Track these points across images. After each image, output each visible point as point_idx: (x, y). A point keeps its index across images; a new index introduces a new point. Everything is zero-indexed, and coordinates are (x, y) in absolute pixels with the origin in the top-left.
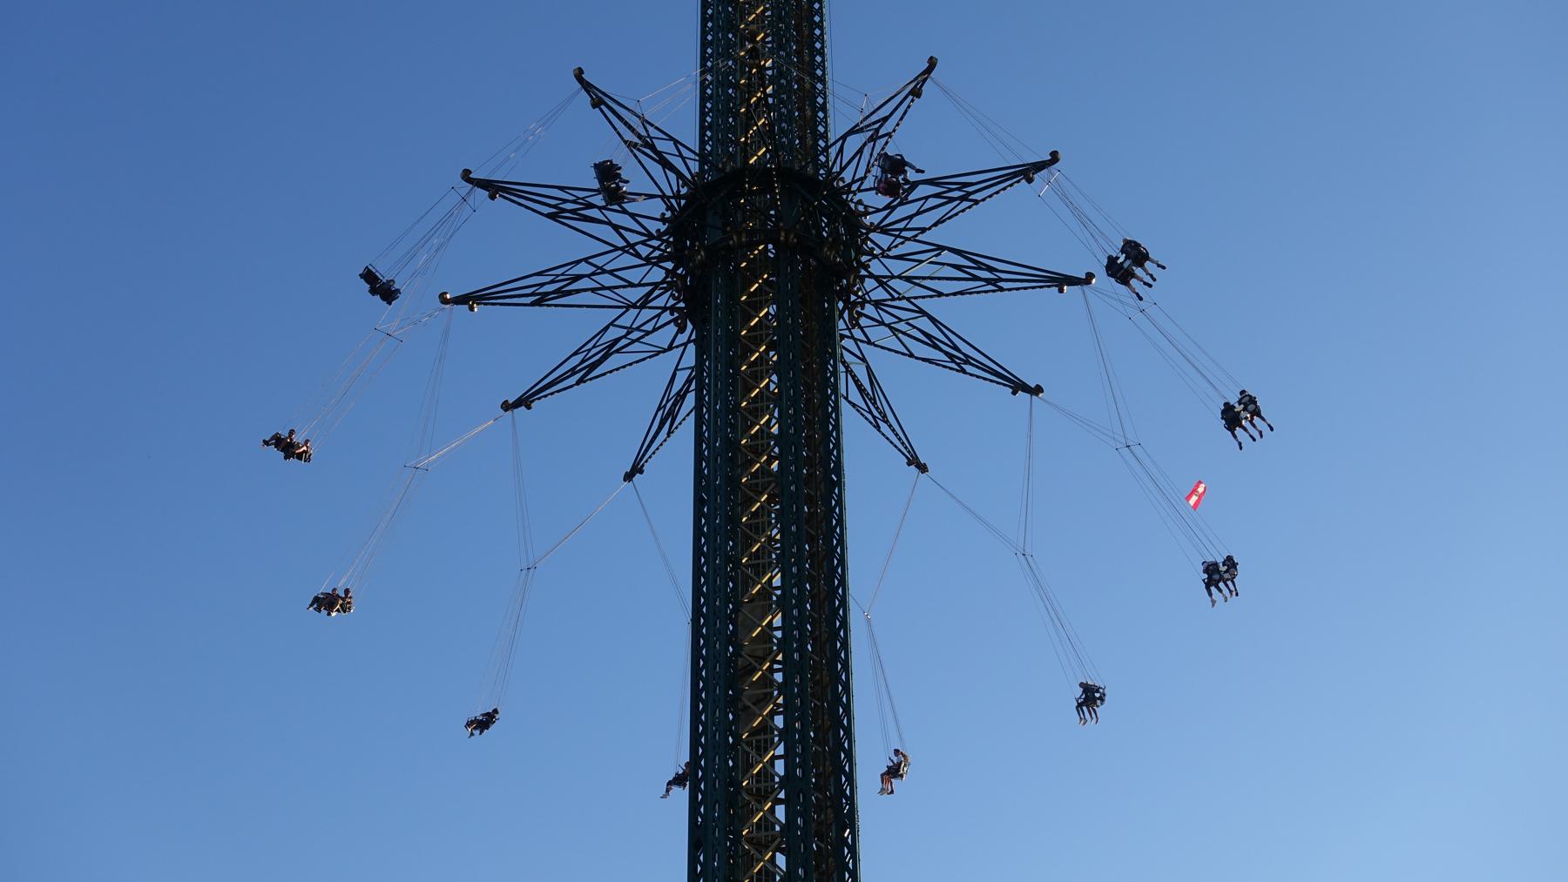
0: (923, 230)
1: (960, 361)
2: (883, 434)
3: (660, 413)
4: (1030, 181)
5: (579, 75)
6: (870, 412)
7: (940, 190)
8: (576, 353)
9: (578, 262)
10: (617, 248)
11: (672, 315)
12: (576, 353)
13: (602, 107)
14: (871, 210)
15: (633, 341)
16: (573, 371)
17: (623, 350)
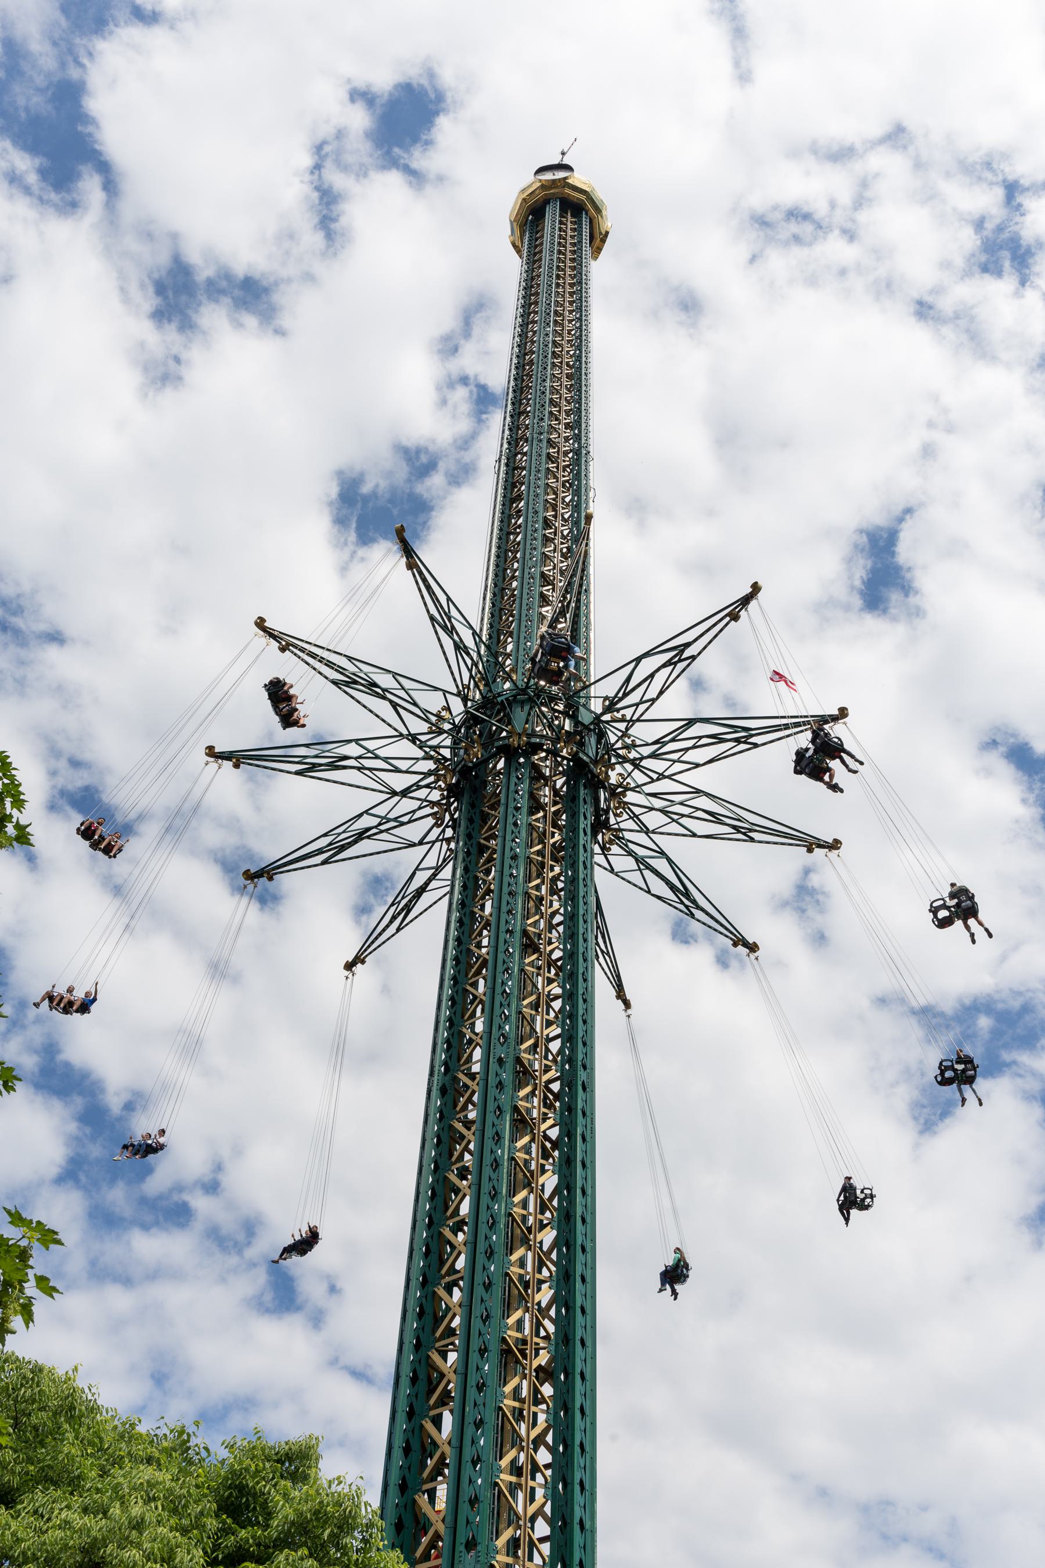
1: (745, 832)
2: (699, 921)
3: (393, 909)
5: (260, 623)
6: (682, 903)
8: (325, 835)
9: (360, 815)
10: (401, 735)
11: (433, 808)
12: (325, 835)
13: (291, 647)
14: (638, 742)
15: (382, 832)
16: (320, 851)
17: (374, 837)
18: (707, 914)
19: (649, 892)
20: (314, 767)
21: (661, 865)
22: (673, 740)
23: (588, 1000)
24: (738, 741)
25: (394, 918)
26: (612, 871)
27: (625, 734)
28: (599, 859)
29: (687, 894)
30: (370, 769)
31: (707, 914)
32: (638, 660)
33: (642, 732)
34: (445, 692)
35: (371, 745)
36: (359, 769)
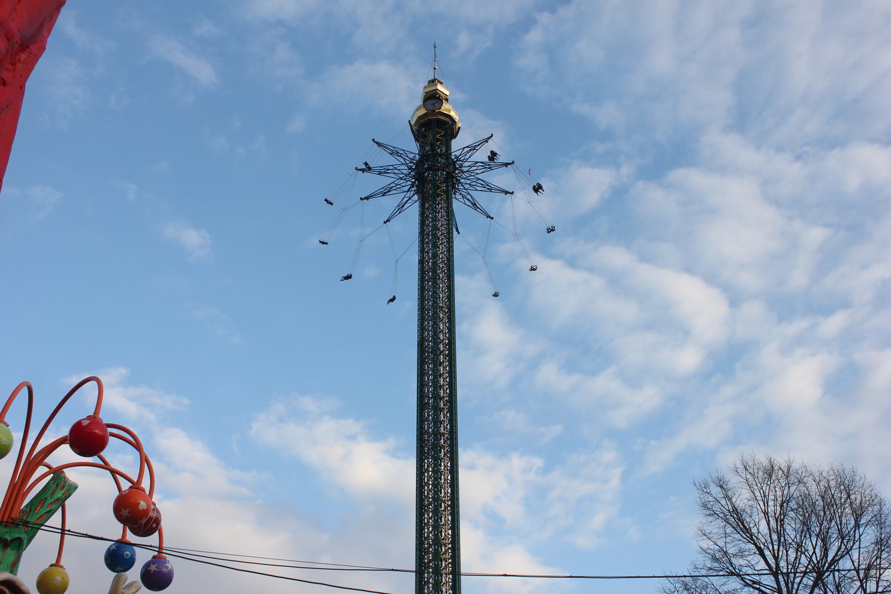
0: (467, 159)
1: (490, 190)
4: (507, 167)
5: (373, 140)
7: (483, 165)
9: (391, 184)
18: (480, 209)
20: (385, 193)
21: (469, 197)
22: (474, 166)
24: (489, 189)
25: (398, 210)
26: (456, 199)
28: (453, 196)
29: (475, 205)
31: (480, 209)
32: (464, 148)
35: (395, 166)
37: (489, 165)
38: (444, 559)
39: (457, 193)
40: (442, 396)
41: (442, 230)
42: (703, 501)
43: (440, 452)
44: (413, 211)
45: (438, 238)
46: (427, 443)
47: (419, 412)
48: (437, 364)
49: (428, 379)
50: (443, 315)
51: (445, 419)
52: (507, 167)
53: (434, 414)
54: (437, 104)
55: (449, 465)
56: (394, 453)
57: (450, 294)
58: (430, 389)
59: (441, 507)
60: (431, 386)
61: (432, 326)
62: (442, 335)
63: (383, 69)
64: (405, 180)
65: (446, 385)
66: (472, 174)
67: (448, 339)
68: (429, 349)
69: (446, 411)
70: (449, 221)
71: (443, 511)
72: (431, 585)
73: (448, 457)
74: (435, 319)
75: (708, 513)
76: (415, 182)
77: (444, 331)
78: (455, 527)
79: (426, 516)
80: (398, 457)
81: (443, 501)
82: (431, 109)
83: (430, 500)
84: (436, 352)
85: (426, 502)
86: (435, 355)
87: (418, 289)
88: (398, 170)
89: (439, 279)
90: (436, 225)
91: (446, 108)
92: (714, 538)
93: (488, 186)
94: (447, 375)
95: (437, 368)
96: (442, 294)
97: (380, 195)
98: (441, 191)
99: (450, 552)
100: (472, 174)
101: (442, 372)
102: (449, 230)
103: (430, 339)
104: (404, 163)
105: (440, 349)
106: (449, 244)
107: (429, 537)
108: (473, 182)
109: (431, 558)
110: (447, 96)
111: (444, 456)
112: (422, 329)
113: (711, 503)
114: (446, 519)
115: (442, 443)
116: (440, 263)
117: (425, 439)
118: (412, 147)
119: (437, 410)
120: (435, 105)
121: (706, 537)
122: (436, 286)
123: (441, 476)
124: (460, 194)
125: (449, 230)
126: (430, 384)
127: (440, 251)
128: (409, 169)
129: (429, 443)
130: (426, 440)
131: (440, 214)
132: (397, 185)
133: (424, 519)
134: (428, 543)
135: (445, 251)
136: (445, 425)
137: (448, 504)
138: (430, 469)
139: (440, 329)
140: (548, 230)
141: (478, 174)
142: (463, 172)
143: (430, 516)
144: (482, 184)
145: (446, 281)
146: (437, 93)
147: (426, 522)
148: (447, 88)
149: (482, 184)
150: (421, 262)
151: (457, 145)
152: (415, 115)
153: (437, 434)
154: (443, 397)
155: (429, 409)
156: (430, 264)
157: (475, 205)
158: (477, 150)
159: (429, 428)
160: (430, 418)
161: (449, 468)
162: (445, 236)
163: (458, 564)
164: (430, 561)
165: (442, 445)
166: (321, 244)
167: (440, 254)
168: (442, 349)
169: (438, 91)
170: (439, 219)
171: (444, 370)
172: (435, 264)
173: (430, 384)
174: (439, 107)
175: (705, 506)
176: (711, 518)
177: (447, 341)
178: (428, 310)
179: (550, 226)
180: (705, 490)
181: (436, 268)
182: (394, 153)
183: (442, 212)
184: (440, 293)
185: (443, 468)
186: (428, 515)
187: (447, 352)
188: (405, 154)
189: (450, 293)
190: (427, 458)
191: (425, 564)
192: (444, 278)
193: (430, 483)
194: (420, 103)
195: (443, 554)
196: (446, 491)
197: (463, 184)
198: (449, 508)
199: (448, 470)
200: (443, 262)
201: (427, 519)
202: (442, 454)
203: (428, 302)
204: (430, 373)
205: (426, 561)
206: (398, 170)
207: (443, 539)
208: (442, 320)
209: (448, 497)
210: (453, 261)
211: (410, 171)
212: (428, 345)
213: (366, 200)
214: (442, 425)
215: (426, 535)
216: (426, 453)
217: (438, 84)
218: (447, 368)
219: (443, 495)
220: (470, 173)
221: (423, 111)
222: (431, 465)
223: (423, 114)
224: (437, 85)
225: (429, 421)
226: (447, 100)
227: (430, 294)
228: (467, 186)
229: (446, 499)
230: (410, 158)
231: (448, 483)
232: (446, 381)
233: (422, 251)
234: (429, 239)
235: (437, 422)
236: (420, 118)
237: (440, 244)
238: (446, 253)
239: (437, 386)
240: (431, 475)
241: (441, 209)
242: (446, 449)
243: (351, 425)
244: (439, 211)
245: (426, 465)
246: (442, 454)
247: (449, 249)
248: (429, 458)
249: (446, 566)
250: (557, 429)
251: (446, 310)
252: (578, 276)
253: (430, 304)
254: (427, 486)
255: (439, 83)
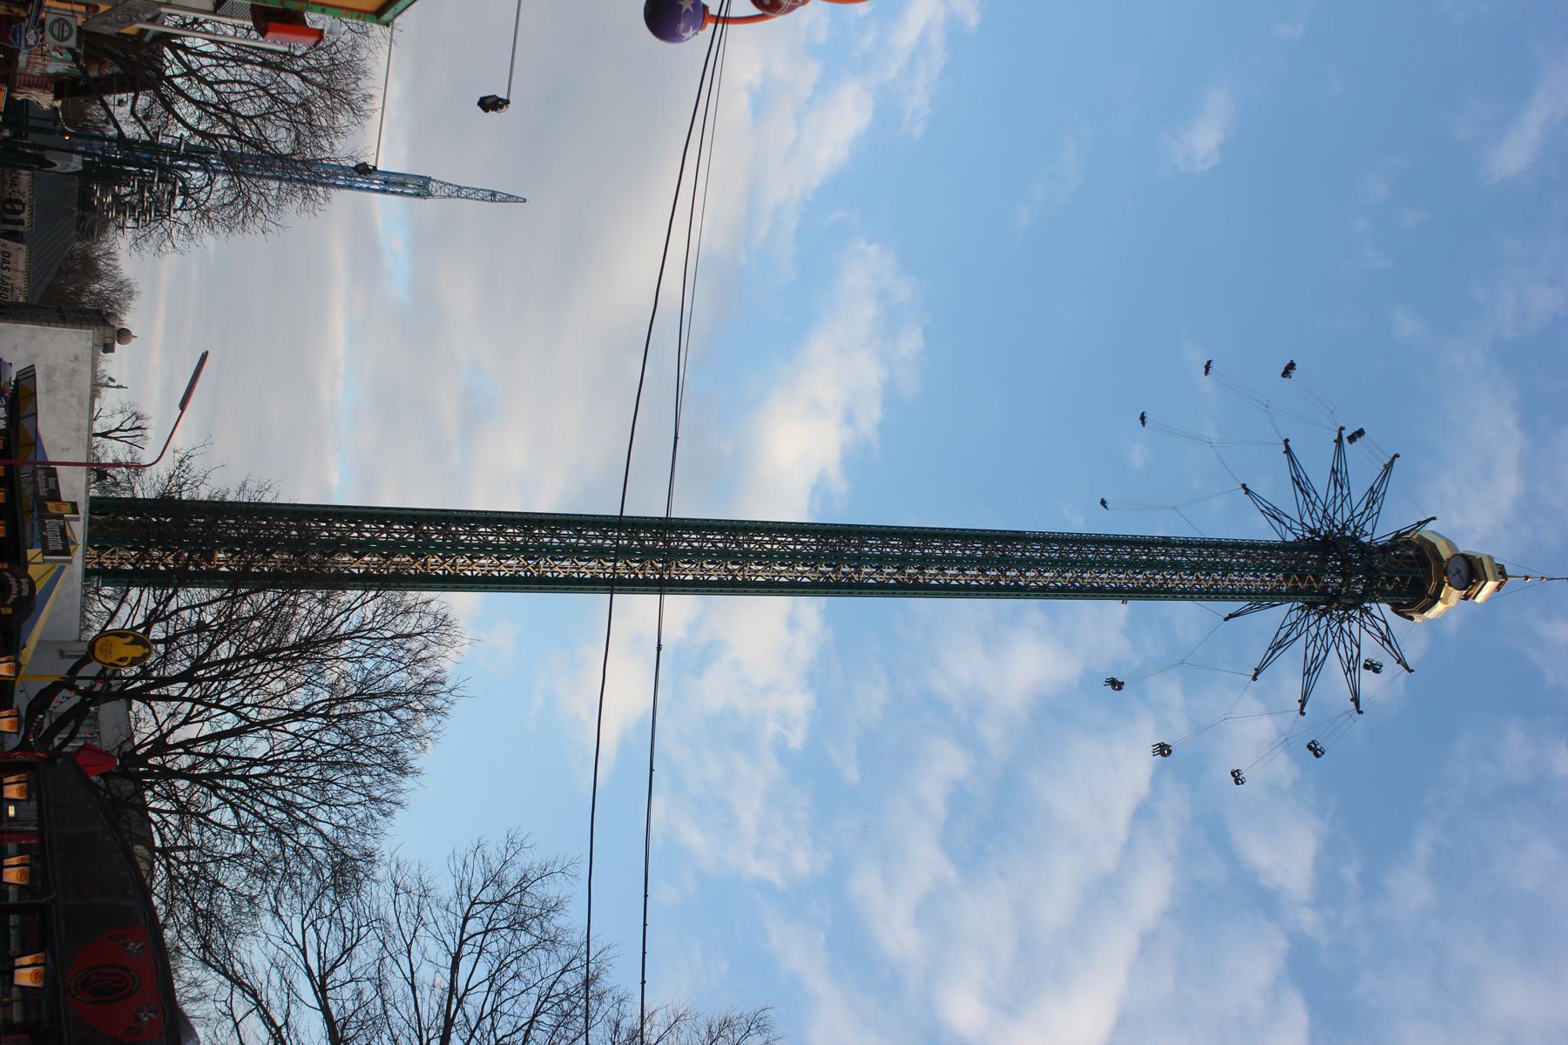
0: (1365, 628)
1: (1307, 673)
4: (1299, 701)
5: (1397, 456)
7: (1355, 658)
12: (1307, 478)
19: (1281, 628)
20: (1298, 484)
21: (1294, 635)
22: (1351, 640)
23: (1233, 599)
24: (1309, 669)
27: (1355, 618)
30: (1335, 502)
32: (1385, 622)
33: (1355, 627)
34: (1372, 534)
35: (1348, 499)
36: (1335, 496)
37: (1354, 669)
38: (643, 566)
39: (1300, 612)
40: (926, 571)
41: (1223, 581)
42: (735, 1022)
43: (827, 566)
44: (1261, 530)
45: (1208, 574)
46: (822, 542)
47: (981, 533)
48: (983, 564)
49: (957, 548)
50: (1070, 578)
51: (885, 576)
52: (1352, 700)
53: (894, 556)
54: (1459, 580)
55: (805, 580)
56: (819, 489)
57: (1107, 591)
58: (938, 551)
59: (733, 563)
60: (943, 553)
61: (1031, 558)
62: (1033, 574)
63: (1508, 485)
64: (1324, 517)
65: (946, 580)
66: (1337, 639)
67: (1027, 586)
68: (1010, 552)
69: (900, 577)
70: (1239, 593)
71: (726, 567)
72: (600, 541)
73: (819, 578)
74: (1063, 564)
75: (713, 1029)
76: (1319, 536)
77: (1040, 579)
78: (734, 587)
79: (719, 537)
80: (812, 495)
81: (743, 568)
82: (1450, 568)
83: (746, 546)
84: (1004, 563)
85: (741, 538)
86: (999, 562)
87: (1100, 535)
88: (1342, 505)
89: (1135, 573)
90: (1232, 570)
91: (1452, 595)
92: (671, 1037)
93: (1316, 669)
94: (942, 582)
95: (955, 564)
96: (1108, 578)
97: (1294, 475)
98: (1294, 580)
99: (654, 577)
100: (1337, 639)
101: (967, 572)
102: (1222, 593)
103: (1027, 554)
104: (1355, 515)
105: (1009, 570)
106: (1197, 593)
107: (707, 542)
108: (1322, 641)
109: (646, 543)
110: (1474, 598)
111: (821, 572)
112: (1045, 539)
113: (731, 1036)
114: (712, 572)
115: (843, 570)
116: (1163, 575)
117: (850, 540)
118: (1382, 530)
119: (902, 562)
120: (1457, 576)
121: (672, 1021)
122: (1085, 566)
123: (786, 565)
124: (1298, 619)
125: (1222, 593)
126: (947, 552)
127: (1186, 577)
128: (1344, 525)
129: (845, 546)
130: (849, 540)
131: (1252, 578)
132: (1314, 504)
133: (713, 534)
134: (672, 540)
135: (1184, 585)
136: (874, 576)
137: (737, 575)
138: (798, 547)
139: (1045, 572)
140: (1237, 771)
141: (1337, 648)
142: (1341, 622)
143: (718, 544)
144: (1317, 657)
145: (1131, 585)
146: (1479, 580)
147: (708, 537)
148: (1489, 599)
149: (1317, 657)
150: (1166, 542)
151: (1383, 610)
152: (1438, 538)
153: (858, 561)
154: (924, 574)
155: (904, 548)
156: (1162, 558)
157: (1277, 646)
158: (1383, 645)
159: (870, 546)
160: (888, 550)
161: (799, 579)
162: (1211, 586)
163: (646, 590)
164: (641, 541)
165: (839, 569)
166: (1206, 363)
167: (1180, 575)
168: (1008, 573)
169: (1483, 582)
170: (1242, 576)
171: (972, 576)
172: (1162, 566)
173: (947, 552)
174: (1452, 582)
175: (727, 1023)
176: (704, 1032)
177: (1022, 583)
178: (1079, 552)
179: (1244, 775)
180: (753, 1026)
181: (1155, 568)
182: (1374, 496)
183: (1270, 581)
184: (1109, 574)
185: (800, 569)
186: (696, 540)
187: (1003, 583)
188: (1371, 515)
189: (1109, 592)
190: (818, 541)
191: (637, 533)
192: (1118, 582)
193: (775, 546)
194: (1462, 550)
195: (652, 564)
196: (760, 573)
197: (1317, 623)
198: (730, 578)
199: (797, 577)
200: (1165, 580)
201: (713, 539)
202: (824, 569)
203: (1093, 552)
204: (968, 552)
205: (642, 535)
206: (1342, 505)
207: (677, 565)
208: (1060, 576)
209: (750, 576)
210: (1166, 598)
211: (1340, 527)
212: (1017, 550)
213: (1285, 450)
214: (874, 570)
215: (686, 536)
216: (827, 539)
217: (1498, 583)
218: (974, 583)
219: (753, 567)
220: (1338, 634)
221: (1445, 553)
222: (805, 549)
223: (1439, 553)
224: (1496, 580)
225: (883, 547)
226: (1466, 597)
227: (1109, 556)
228: (1313, 630)
229: (746, 573)
230: (1364, 524)
231: (773, 577)
232: (952, 580)
233: (1187, 544)
234: (1208, 556)
235: (880, 561)
236: (1433, 546)
237: (1197, 577)
238: (1182, 586)
239: (943, 563)
240: (789, 548)
241: (1262, 580)
242: (833, 576)
243: (871, 415)
244: (1274, 577)
245: (807, 540)
246: (824, 569)
247: (1189, 593)
248: (817, 546)
249: (632, 569)
250: (852, 775)
251: (1077, 584)
252: (1119, 821)
253: (1090, 556)
254: (770, 540)
255: (1500, 585)
